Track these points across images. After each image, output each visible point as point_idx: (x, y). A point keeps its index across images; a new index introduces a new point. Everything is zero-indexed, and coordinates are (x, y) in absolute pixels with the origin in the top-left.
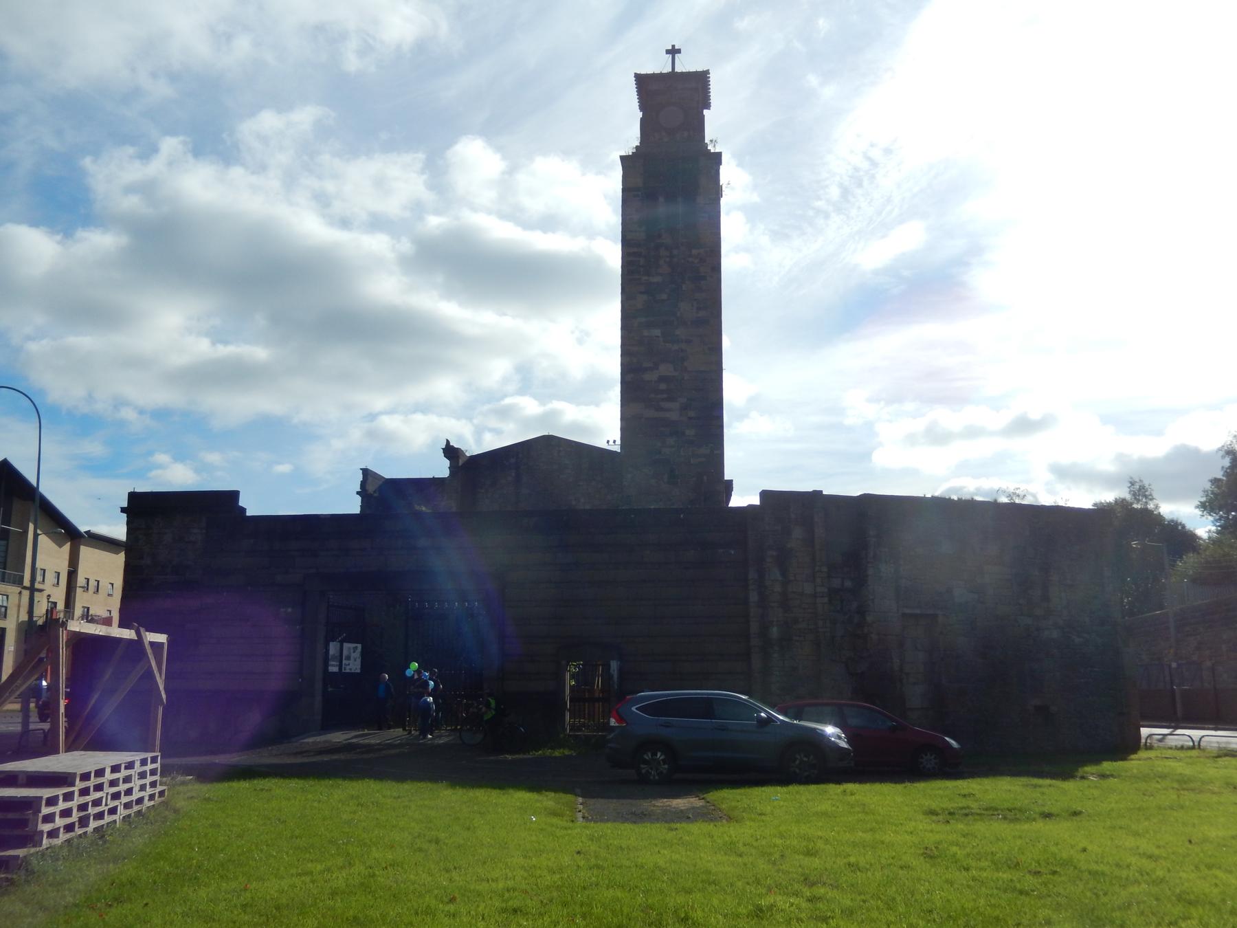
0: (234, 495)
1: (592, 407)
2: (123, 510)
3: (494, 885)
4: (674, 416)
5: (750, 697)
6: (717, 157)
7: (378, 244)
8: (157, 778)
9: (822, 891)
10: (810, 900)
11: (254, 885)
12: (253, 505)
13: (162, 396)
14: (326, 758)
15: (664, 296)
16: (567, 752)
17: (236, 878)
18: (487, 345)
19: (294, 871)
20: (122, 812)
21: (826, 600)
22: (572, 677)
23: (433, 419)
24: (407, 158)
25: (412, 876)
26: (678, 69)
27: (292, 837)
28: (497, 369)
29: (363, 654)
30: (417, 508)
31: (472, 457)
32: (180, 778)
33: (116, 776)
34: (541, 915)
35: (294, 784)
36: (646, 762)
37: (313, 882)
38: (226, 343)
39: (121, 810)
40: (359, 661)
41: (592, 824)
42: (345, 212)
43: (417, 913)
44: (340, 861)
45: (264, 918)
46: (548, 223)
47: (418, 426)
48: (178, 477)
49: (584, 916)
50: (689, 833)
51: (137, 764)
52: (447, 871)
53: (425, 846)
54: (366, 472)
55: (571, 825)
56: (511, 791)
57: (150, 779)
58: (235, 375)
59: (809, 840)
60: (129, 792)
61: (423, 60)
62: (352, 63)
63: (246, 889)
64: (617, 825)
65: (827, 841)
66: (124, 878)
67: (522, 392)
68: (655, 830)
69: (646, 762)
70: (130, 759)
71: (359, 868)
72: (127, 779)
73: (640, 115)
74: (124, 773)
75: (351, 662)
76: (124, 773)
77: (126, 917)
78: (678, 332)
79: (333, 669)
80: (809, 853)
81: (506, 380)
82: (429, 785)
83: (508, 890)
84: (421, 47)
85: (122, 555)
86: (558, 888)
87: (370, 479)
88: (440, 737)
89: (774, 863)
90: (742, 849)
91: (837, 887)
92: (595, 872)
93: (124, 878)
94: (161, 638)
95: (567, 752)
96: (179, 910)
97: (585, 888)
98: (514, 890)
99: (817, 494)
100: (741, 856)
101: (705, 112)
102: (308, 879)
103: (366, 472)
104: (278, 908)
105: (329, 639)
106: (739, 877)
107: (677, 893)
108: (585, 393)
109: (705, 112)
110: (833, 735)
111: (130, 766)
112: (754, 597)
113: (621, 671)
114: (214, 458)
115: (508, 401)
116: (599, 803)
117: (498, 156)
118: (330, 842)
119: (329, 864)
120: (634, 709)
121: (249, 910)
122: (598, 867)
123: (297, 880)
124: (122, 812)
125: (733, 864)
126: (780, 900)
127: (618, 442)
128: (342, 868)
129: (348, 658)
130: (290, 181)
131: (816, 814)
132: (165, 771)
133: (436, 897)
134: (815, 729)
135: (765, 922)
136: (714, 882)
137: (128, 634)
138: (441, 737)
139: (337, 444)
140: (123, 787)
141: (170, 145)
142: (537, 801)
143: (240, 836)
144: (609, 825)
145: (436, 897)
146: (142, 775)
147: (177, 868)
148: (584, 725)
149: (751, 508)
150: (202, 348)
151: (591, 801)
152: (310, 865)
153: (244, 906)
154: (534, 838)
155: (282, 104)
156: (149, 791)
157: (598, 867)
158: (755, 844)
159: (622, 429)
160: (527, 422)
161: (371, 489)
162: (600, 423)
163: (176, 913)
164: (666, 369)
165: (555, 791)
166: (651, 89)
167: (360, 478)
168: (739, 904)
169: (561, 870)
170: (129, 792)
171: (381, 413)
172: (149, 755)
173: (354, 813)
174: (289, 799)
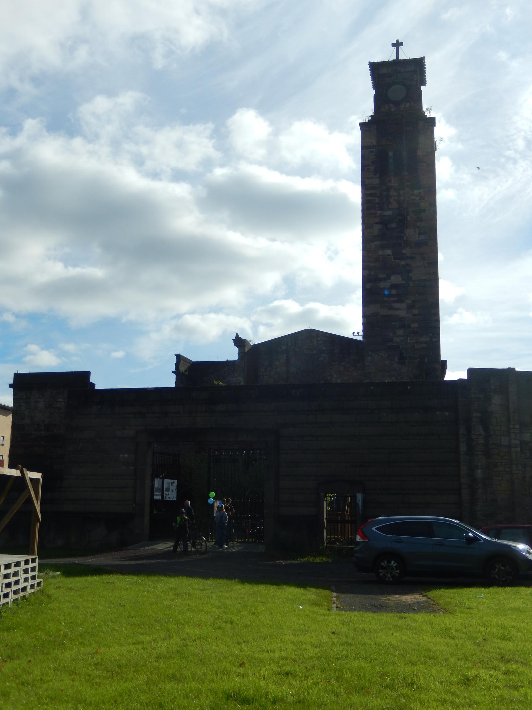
0: (87, 374)
1: (340, 306)
2: (11, 386)
3: (272, 655)
4: (402, 313)
5: (461, 521)
6: (432, 122)
7: (181, 190)
8: (35, 573)
9: (514, 667)
10: (505, 673)
11: (103, 650)
12: (101, 381)
13: (30, 305)
14: (133, 562)
15: (394, 225)
16: (325, 559)
17: (90, 645)
18: (262, 262)
19: (130, 641)
20: (12, 596)
21: (518, 449)
22: (329, 505)
23: (222, 317)
24: (200, 127)
25: (214, 647)
26: (401, 57)
27: (129, 617)
28: (270, 280)
29: (178, 487)
30: (216, 382)
31: (255, 346)
32: (51, 574)
33: (8, 571)
34: (306, 677)
35: (131, 579)
36: (383, 568)
37: (144, 649)
38: (75, 266)
39: (11, 595)
40: (175, 492)
41: (343, 613)
42: (157, 170)
43: (217, 674)
44: (163, 634)
45: (110, 674)
46: (305, 170)
47: (216, 322)
48: (45, 360)
49: (337, 680)
50: (415, 621)
51: (22, 563)
52: (239, 643)
53: (223, 625)
54: (179, 357)
55: (328, 612)
56: (284, 587)
57: (31, 574)
58: (82, 288)
59: (505, 628)
60: (17, 583)
61: (211, 57)
62: (159, 62)
63: (97, 652)
64: (361, 613)
65: (519, 630)
66: (14, 642)
67: (286, 297)
68: (390, 618)
69: (383, 568)
70: (17, 560)
71: (176, 640)
72: (16, 574)
73: (374, 92)
74: (13, 569)
75: (170, 493)
76: (13, 569)
77: (16, 669)
78: (404, 252)
79: (157, 497)
80: (505, 638)
81: (276, 288)
82: (225, 581)
83: (282, 659)
84: (210, 50)
85: (10, 417)
86: (318, 658)
87: (182, 361)
88: (233, 547)
89: (478, 645)
90: (455, 634)
91: (526, 664)
92: (345, 647)
93: (14, 642)
94: (38, 476)
95: (325, 559)
96: (52, 666)
97: (338, 659)
98: (287, 659)
99: (511, 370)
100: (453, 638)
101: (422, 88)
102: (140, 647)
103: (179, 357)
104: (119, 667)
105: (155, 475)
106: (452, 655)
107: (405, 665)
108: (336, 295)
109: (422, 88)
110: (523, 550)
111: (17, 564)
112: (463, 447)
113: (364, 501)
114: (70, 347)
115: (276, 303)
116: (348, 597)
117: (267, 124)
118: (156, 621)
119: (155, 636)
120: (374, 529)
121: (99, 667)
122: (347, 644)
123: (131, 647)
124: (12, 596)
125: (447, 644)
126: (484, 673)
127: (361, 333)
128: (164, 639)
129: (168, 490)
130: (116, 145)
131: (511, 609)
132: (42, 568)
133: (230, 662)
134: (510, 546)
135: (470, 688)
136: (433, 658)
137: (15, 473)
138: (233, 547)
139: (154, 336)
140: (12, 579)
141: (31, 125)
142: (303, 594)
143: (92, 615)
144: (356, 613)
145: (230, 662)
146: (26, 571)
147: (50, 636)
148: (337, 540)
149: (461, 381)
150: (58, 270)
151: (343, 596)
152: (141, 637)
153: (96, 665)
154: (301, 621)
155: (111, 93)
156: (31, 582)
157: (347, 644)
158: (464, 630)
159: (364, 324)
160: (292, 319)
161: (182, 369)
162: (348, 320)
163: (50, 668)
164: (396, 279)
165: (317, 587)
166: (380, 72)
167: (175, 361)
168: (452, 674)
169: (320, 645)
170: (17, 583)
171: (185, 314)
172: (30, 557)
173: (173, 600)
174: (127, 589)
